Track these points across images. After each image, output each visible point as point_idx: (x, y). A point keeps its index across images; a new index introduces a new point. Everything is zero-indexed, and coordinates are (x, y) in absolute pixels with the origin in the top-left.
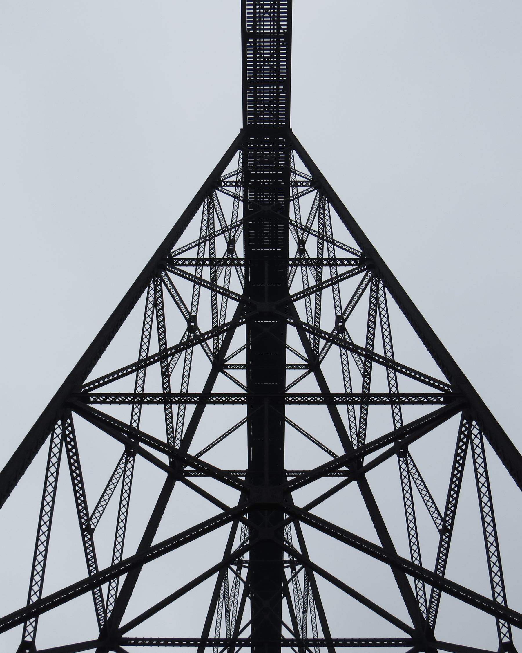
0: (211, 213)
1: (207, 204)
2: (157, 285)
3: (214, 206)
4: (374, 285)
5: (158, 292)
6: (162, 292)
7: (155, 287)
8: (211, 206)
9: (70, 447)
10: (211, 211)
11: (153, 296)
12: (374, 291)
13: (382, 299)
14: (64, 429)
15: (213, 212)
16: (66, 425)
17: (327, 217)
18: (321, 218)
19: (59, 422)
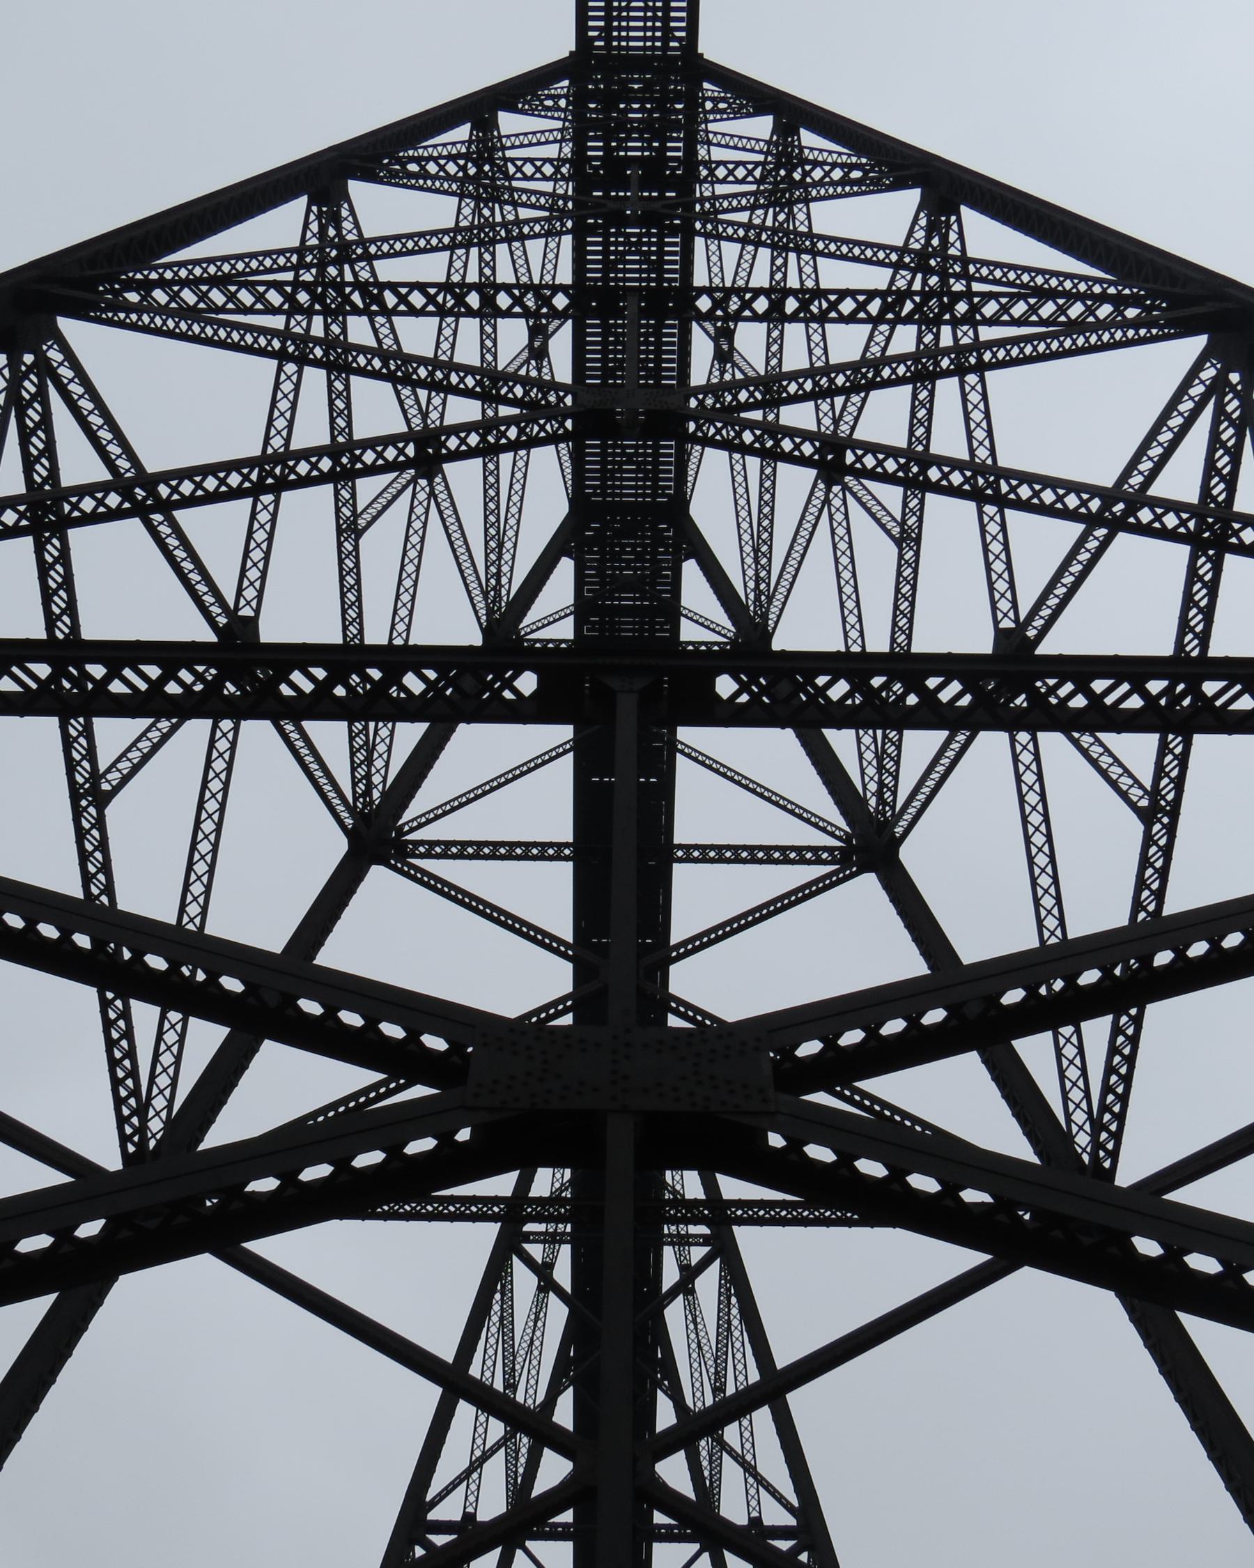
0: (492, 577)
1: (501, 598)
2: (494, 589)
3: (485, 594)
4: (888, 804)
5: (363, 777)
6: (353, 777)
7: (368, 792)
8: (492, 593)
9: (129, 1082)
10: (493, 582)
11: (373, 770)
12: (889, 789)
13: (871, 771)
14: (142, 1129)
15: (487, 580)
16: (136, 1139)
17: (750, 573)
18: (765, 569)
19: (152, 1143)
